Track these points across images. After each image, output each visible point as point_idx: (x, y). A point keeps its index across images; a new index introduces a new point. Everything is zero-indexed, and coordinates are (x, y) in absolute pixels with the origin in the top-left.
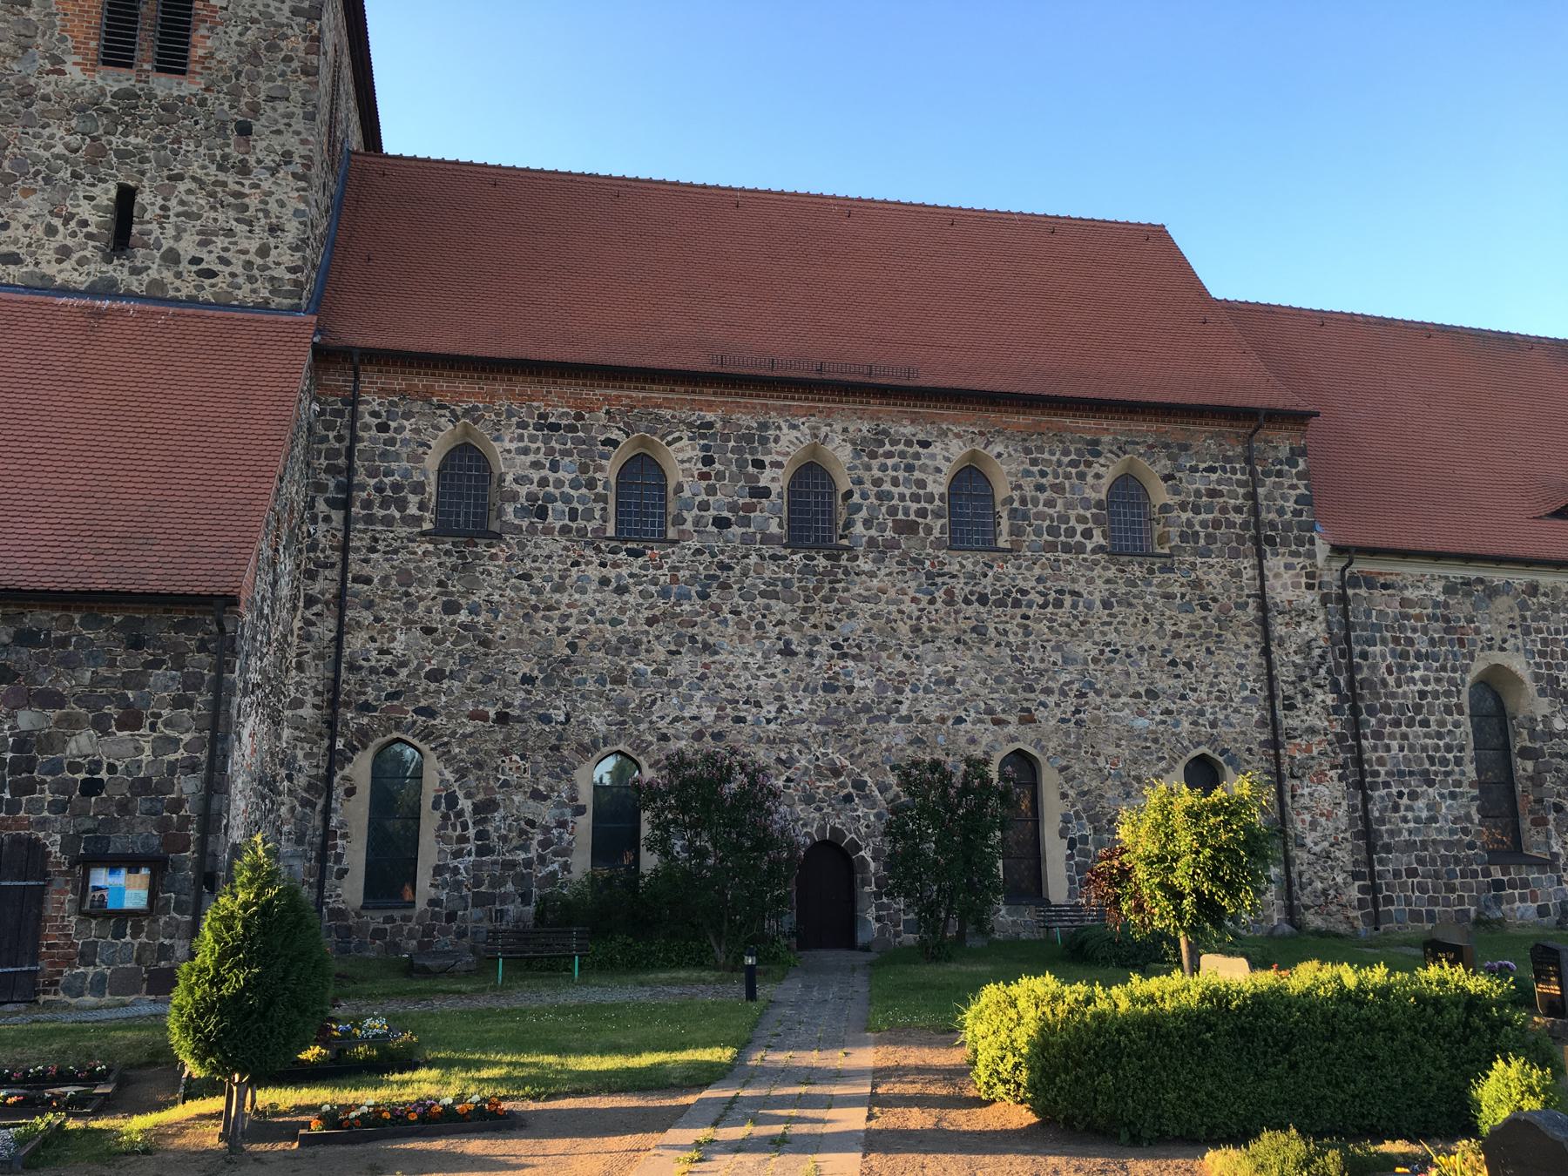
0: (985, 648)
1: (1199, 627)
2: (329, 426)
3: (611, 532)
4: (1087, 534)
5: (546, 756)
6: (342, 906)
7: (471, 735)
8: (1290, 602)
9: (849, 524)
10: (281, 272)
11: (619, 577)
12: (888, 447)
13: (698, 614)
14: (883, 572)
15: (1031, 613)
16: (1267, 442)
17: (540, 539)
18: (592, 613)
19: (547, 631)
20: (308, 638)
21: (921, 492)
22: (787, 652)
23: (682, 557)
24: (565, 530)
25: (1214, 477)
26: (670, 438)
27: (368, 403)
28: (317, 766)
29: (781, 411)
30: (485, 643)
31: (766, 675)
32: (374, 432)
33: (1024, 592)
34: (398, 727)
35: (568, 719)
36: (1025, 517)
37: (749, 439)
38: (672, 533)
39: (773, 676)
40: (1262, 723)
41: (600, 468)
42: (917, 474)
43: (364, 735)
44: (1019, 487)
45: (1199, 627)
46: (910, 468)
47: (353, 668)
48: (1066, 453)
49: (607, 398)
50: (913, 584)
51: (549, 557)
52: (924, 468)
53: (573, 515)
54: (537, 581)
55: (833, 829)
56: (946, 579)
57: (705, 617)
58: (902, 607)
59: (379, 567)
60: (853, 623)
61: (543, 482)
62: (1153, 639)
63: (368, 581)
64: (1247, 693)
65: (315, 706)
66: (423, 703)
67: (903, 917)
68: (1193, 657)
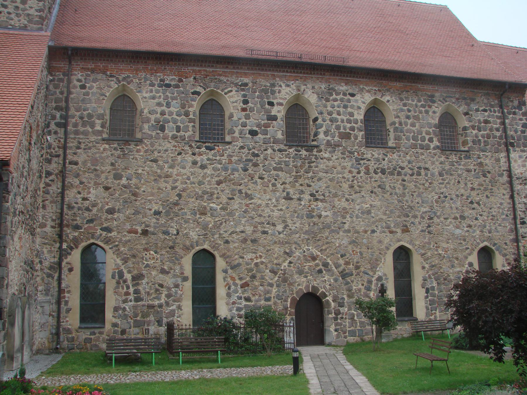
0: (385, 196)
1: (482, 185)
2: (56, 87)
3: (197, 139)
4: (431, 140)
5: (167, 252)
6: (70, 327)
7: (129, 241)
8: (522, 174)
9: (316, 134)
10: (32, 12)
11: (202, 160)
12: (334, 96)
13: (243, 179)
14: (335, 157)
15: (406, 178)
16: (509, 98)
17: (161, 141)
18: (188, 178)
19: (166, 188)
20: (47, 192)
21: (352, 118)
22: (288, 198)
23: (234, 150)
24: (174, 137)
25: (486, 114)
26: (226, 91)
27: (75, 75)
28: (54, 257)
29: (281, 77)
30: (135, 194)
31: (278, 210)
32: (78, 89)
33: (403, 168)
34: (93, 238)
35: (178, 233)
36: (402, 131)
37: (265, 91)
38: (228, 138)
39: (281, 210)
40: (511, 231)
41: (192, 106)
42: (349, 110)
43: (76, 242)
44: (398, 117)
45: (482, 185)
46: (345, 107)
47: (70, 207)
48: (419, 101)
49: (193, 70)
50: (350, 164)
51: (166, 151)
52: (352, 107)
53: (178, 129)
54: (160, 163)
55: (313, 287)
56: (365, 161)
57: (246, 180)
58: (345, 175)
59: (82, 157)
60: (320, 183)
61: (163, 113)
62: (462, 191)
63: (76, 163)
64: (504, 216)
65: (52, 227)
66: (105, 225)
67: (348, 329)
68: (480, 200)
